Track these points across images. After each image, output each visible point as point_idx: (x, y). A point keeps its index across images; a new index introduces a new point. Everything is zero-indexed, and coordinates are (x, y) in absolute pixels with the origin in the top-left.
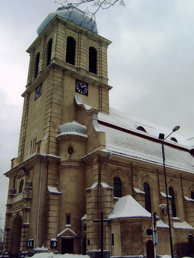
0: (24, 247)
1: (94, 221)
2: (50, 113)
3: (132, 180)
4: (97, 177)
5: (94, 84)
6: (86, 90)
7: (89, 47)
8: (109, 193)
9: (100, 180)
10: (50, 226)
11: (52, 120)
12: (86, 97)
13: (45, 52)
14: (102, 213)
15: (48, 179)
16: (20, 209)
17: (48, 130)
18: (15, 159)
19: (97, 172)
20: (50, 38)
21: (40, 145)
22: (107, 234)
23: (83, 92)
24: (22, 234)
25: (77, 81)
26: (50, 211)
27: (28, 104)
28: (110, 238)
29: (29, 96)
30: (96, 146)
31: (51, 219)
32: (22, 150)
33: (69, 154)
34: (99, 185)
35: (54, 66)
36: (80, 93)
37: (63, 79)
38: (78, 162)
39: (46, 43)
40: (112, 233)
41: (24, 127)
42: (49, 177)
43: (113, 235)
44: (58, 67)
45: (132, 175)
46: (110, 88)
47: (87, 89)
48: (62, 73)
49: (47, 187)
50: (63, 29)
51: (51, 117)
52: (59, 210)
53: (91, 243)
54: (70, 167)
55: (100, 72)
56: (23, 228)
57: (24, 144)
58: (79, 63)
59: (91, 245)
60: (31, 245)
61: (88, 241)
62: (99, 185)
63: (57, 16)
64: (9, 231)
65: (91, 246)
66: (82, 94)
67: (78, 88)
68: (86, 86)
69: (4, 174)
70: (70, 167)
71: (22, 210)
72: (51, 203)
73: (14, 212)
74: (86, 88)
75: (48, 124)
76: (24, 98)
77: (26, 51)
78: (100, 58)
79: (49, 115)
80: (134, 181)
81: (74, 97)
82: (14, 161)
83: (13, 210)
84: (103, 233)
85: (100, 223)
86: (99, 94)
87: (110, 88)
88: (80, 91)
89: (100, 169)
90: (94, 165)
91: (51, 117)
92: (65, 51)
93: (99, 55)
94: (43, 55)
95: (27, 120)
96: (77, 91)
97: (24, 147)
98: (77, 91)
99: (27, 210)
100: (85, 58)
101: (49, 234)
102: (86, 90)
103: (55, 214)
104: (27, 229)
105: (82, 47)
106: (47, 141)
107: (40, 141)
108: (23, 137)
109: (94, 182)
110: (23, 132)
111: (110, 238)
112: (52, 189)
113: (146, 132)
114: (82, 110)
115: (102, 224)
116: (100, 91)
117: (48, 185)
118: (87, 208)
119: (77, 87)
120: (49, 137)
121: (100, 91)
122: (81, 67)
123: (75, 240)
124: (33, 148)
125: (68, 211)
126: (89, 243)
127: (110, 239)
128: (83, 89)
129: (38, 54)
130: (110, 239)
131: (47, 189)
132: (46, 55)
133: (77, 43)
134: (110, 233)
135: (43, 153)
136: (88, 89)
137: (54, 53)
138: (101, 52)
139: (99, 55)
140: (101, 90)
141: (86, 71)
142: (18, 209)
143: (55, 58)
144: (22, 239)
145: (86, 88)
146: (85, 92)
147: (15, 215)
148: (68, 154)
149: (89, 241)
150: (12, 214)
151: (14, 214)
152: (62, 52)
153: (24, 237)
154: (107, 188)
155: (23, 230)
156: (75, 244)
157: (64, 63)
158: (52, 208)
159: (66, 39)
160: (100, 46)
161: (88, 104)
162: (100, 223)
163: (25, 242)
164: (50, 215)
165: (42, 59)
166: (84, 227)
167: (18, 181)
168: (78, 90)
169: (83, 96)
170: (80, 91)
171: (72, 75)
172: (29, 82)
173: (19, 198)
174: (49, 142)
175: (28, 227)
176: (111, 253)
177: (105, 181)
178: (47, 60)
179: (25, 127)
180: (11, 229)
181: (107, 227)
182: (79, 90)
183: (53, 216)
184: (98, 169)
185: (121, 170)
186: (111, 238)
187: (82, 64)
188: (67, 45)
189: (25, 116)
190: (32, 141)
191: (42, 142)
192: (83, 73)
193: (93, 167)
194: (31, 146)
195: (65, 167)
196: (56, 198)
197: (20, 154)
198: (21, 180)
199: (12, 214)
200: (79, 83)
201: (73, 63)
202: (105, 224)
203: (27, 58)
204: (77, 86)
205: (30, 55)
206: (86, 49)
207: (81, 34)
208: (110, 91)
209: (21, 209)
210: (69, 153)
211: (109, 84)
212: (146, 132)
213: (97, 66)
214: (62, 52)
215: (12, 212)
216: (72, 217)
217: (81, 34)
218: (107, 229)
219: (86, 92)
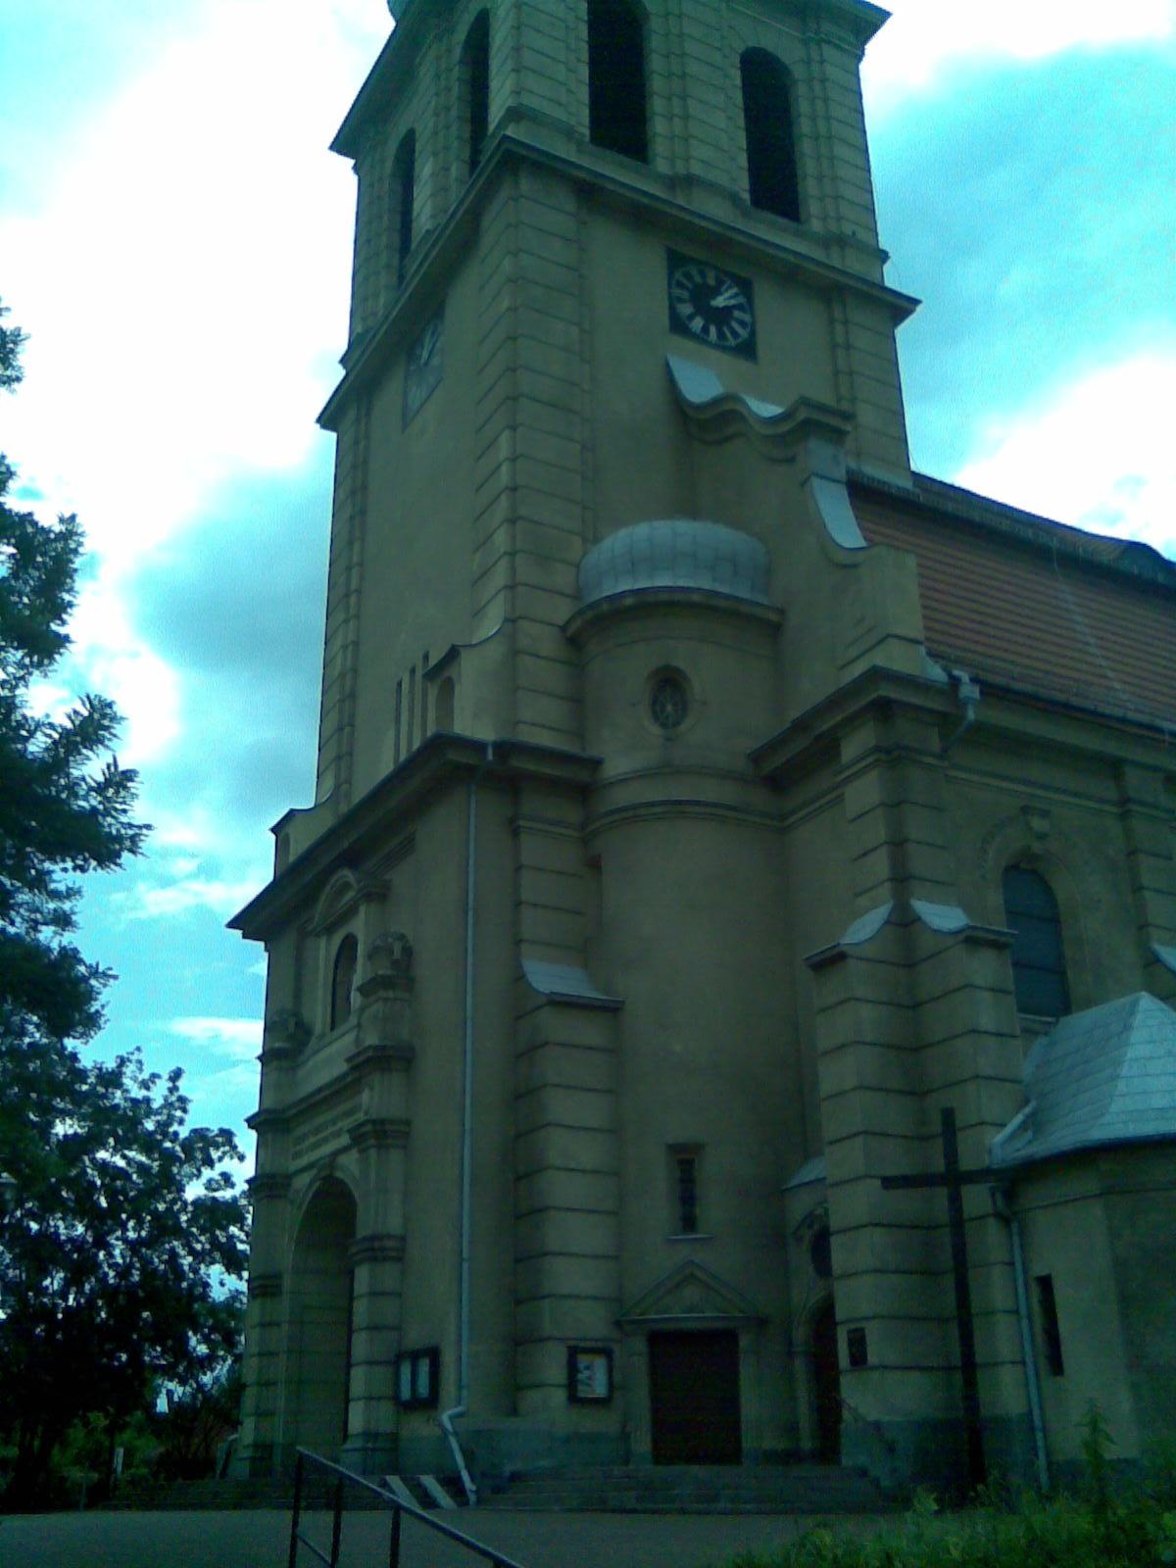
0: (374, 1403)
1: (888, 1183)
2: (504, 469)
3: (1138, 889)
4: (880, 865)
5: (792, 276)
6: (743, 324)
7: (741, 48)
8: (985, 968)
9: (902, 880)
11: (523, 511)
12: (743, 365)
13: (448, 109)
14: (948, 1115)
16: (337, 1134)
17: (499, 577)
18: (298, 816)
19: (877, 831)
20: (479, 7)
21: (454, 676)
22: (998, 1276)
23: (721, 335)
24: (361, 1310)
25: (675, 260)
27: (365, 462)
28: (1023, 1311)
29: (368, 414)
30: (853, 652)
31: (561, 1189)
32: (339, 758)
33: (664, 725)
34: (904, 922)
35: (515, 161)
36: (701, 338)
38: (726, 775)
39: (449, 51)
40: (1039, 1270)
41: (347, 608)
42: (526, 894)
43: (1046, 1283)
44: (543, 166)
45: (1132, 853)
46: (901, 307)
47: (747, 318)
49: (519, 966)
51: (514, 489)
53: (872, 1358)
54: (676, 809)
56: (360, 1262)
57: (352, 716)
59: (874, 1368)
60: (423, 1389)
61: (851, 1343)
62: (904, 922)
64: (273, 1295)
65: (876, 1375)
66: (716, 346)
67: (686, 309)
68: (736, 295)
69: (232, 925)
70: (676, 809)
71: (358, 1138)
73: (304, 1161)
74: (740, 307)
75: (501, 540)
76: (333, 436)
77: (332, 148)
79: (504, 476)
80: (1147, 894)
81: (668, 365)
82: (291, 830)
83: (298, 1148)
84: (972, 1274)
85: (941, 1195)
86: (834, 346)
87: (901, 307)
88: (705, 330)
89: (894, 805)
90: (849, 780)
91: (514, 489)
92: (584, 71)
93: (813, 101)
94: (436, 133)
95: (361, 564)
96: (678, 326)
97: (352, 734)
98: (678, 326)
99: (379, 1134)
101: (549, 1296)
102: (743, 324)
103: (588, 1152)
104: (389, 1274)
105: (690, 47)
106: (496, 652)
107: (453, 654)
108: (342, 675)
109: (863, 901)
110: (338, 642)
111: (1023, 1311)
112: (547, 976)
114: (729, 439)
115: (955, 1200)
116: (839, 328)
117: (525, 948)
118: (826, 1087)
119: (680, 300)
120: (511, 620)
121: (839, 328)
122: (696, 169)
123: (744, 1342)
124: (410, 725)
126: (859, 1360)
127: (1025, 1323)
128: (722, 317)
129: (408, 145)
130: (1030, 1318)
131: (520, 977)
132: (454, 129)
134: (1025, 1271)
135: (474, 721)
136: (753, 315)
137: (509, 85)
138: (823, 80)
139: (813, 119)
140: (846, 322)
141: (734, 199)
142: (325, 1140)
143: (515, 114)
144: (361, 1345)
145: (740, 307)
146: (735, 334)
147: (311, 1184)
148: (655, 730)
149: (858, 1341)
150: (289, 1177)
151: (302, 1181)
152: (561, 72)
153: (373, 1328)
154: (969, 933)
155: (363, 1275)
156: (747, 1373)
157: (579, 144)
158: (561, 1106)
160: (805, 42)
161: (764, 398)
162: (941, 1195)
163: (378, 1363)
165: (435, 154)
166: (808, 1235)
167: (324, 951)
168: (691, 317)
169: (726, 359)
170: (705, 330)
171: (641, 217)
172: (359, 329)
173: (326, 1064)
174: (515, 653)
175: (400, 1259)
176: (1044, 1430)
177: (944, 889)
178: (467, 135)
179: (352, 611)
180: (287, 1283)
181: (993, 1227)
182: (697, 324)
184: (882, 804)
185: (1045, 814)
186: (1036, 1308)
187: (700, 151)
189: (350, 543)
190: (400, 684)
191: (464, 654)
192: (716, 209)
193: (840, 798)
194: (398, 720)
195: (634, 815)
196: (590, 1031)
197: (329, 783)
198: (337, 939)
199: (289, 1177)
200: (688, 276)
202: (977, 1199)
203: (341, 179)
204: (677, 292)
205: (356, 168)
206: (717, 58)
208: (904, 332)
209: (345, 1140)
210: (657, 715)
211: (894, 277)
214: (561, 72)
215: (293, 1166)
216: (712, 1169)
218: (990, 1241)
219: (743, 333)
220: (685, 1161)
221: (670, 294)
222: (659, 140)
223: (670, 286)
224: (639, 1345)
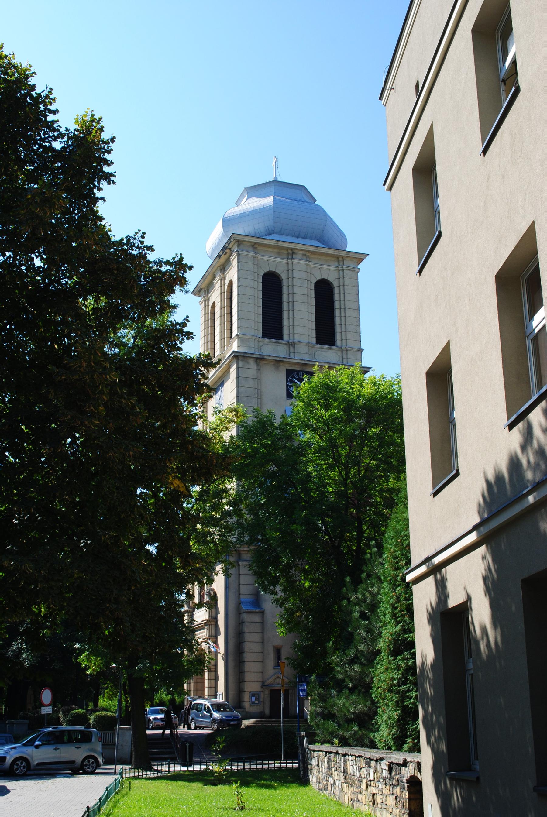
10: (246, 679)
15: (241, 586)
26: (245, 703)
37: (258, 379)
48: (255, 367)
50: (251, 249)
52: (263, 642)
55: (341, 319)
58: (291, 331)
63: (234, 236)
72: (247, 628)
78: (344, 341)
100: (305, 291)
113: (432, 125)
125: (278, 643)
133: (285, 283)
158: (248, 637)
159: (260, 280)
164: (245, 649)
183: (251, 651)
187: (298, 330)
188: (263, 288)
201: (279, 336)
207: (292, 259)
212: (432, 125)
213: (335, 332)
217: (292, 259)
220: (278, 651)
221: (287, 385)
222: (284, 287)
223: (287, 382)
224: (267, 692)
